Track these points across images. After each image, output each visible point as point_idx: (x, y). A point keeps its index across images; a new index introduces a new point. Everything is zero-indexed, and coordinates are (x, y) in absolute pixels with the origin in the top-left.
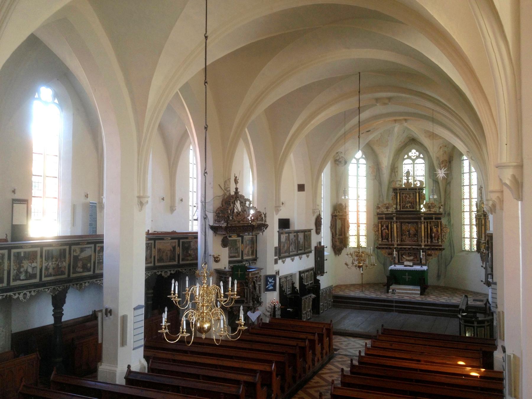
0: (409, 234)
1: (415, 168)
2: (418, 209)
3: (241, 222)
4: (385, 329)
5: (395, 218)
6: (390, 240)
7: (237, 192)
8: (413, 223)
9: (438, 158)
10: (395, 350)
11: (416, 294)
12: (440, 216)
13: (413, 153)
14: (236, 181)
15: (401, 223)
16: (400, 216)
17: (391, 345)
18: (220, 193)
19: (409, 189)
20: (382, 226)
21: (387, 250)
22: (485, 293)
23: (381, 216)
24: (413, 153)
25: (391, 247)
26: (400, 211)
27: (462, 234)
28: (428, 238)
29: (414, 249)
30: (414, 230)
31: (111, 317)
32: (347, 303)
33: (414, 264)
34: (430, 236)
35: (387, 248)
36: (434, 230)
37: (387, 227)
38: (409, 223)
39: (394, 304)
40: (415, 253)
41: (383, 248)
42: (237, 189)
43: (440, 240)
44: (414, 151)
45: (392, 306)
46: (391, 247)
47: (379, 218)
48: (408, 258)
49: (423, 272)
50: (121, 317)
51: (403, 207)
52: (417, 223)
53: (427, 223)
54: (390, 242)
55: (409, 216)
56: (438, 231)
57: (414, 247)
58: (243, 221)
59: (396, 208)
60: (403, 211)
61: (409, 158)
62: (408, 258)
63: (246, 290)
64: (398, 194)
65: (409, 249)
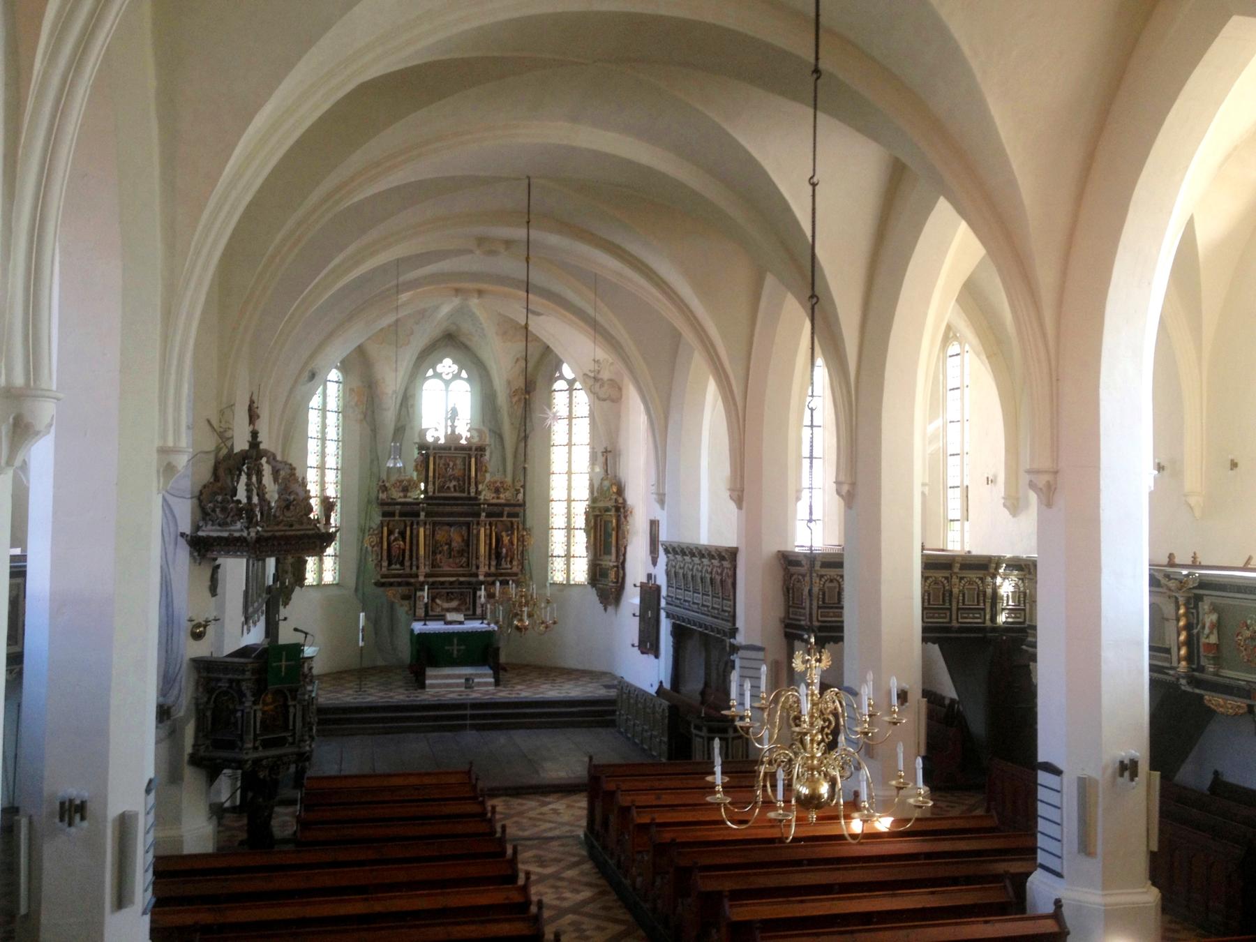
0: (451, 550)
1: (574, 400)
2: (473, 494)
3: (296, 527)
4: (596, 767)
5: (423, 514)
6: (407, 563)
7: (254, 442)
8: (460, 524)
9: (509, 383)
10: (672, 807)
11: (486, 684)
12: (517, 509)
13: (447, 366)
14: (253, 416)
15: (434, 524)
16: (436, 509)
17: (658, 798)
18: (210, 443)
19: (456, 449)
20: (390, 533)
21: (400, 589)
22: (603, 669)
23: (391, 509)
24: (447, 366)
25: (412, 580)
26: (431, 498)
27: (547, 547)
28: (490, 559)
29: (461, 583)
30: (460, 540)
31: (85, 824)
32: (349, 721)
33: (468, 618)
34: (496, 554)
35: (399, 584)
36: (506, 540)
37: (403, 534)
38: (450, 525)
39: (468, 712)
40: (462, 594)
41: (391, 584)
42: (255, 434)
43: (515, 563)
44: (448, 361)
45: (463, 717)
46: (412, 580)
47: (385, 514)
48: (446, 605)
49: (489, 634)
50: (114, 821)
51: (441, 489)
52: (468, 525)
53: (490, 524)
54: (408, 571)
55: (455, 509)
56: (511, 542)
57: (462, 579)
58: (302, 524)
59: (426, 491)
60: (436, 498)
61: (438, 375)
62: (446, 605)
63: (292, 710)
64: (473, 460)
65: (451, 583)
